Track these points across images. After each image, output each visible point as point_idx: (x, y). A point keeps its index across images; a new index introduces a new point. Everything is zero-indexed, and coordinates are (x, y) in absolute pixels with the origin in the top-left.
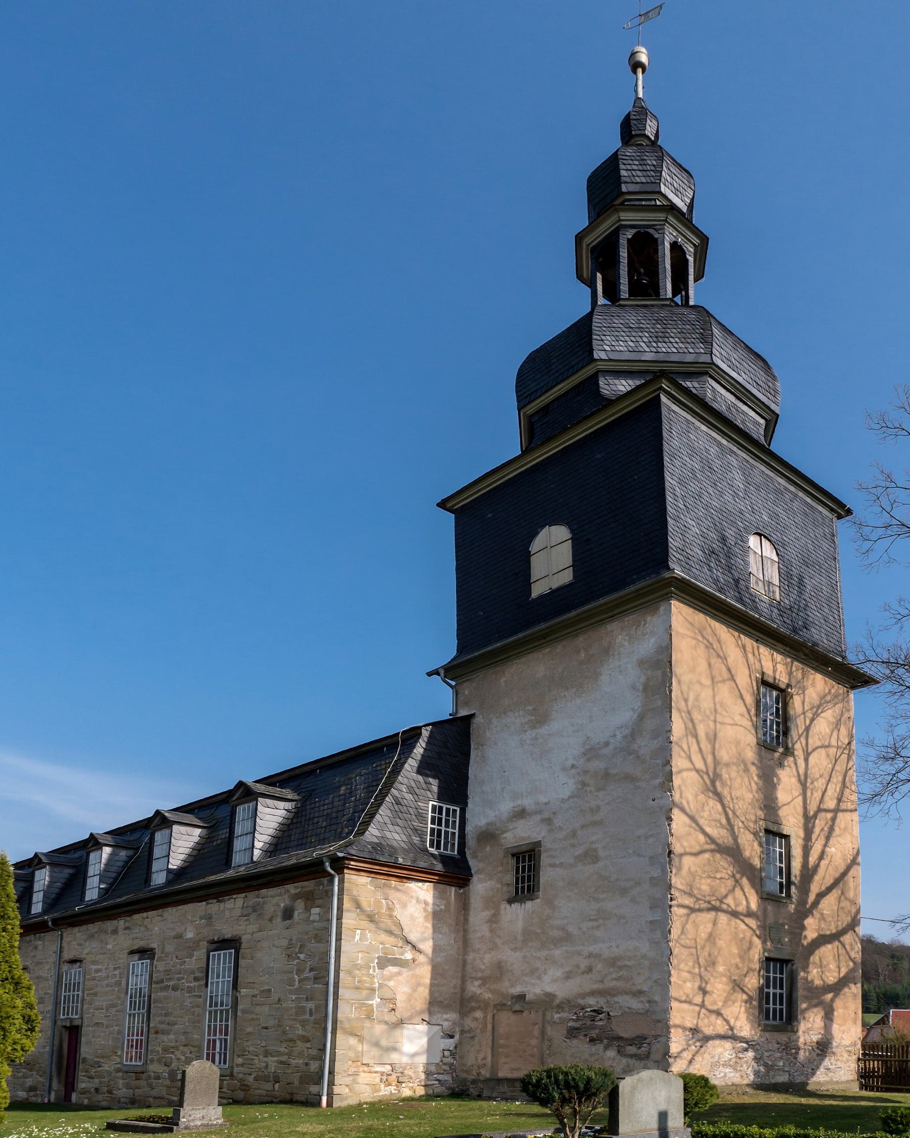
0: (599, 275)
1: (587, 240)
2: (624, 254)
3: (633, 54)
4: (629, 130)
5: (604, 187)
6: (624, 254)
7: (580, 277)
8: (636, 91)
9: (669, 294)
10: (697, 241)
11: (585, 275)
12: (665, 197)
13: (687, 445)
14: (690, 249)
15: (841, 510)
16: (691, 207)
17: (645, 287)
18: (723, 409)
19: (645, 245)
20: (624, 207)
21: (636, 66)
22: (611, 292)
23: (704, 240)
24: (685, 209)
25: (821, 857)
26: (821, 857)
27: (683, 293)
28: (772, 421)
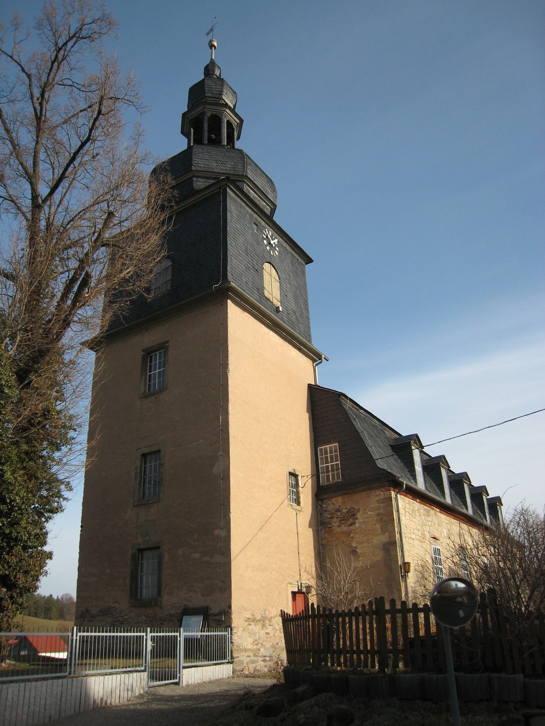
0: (192, 130)
1: (188, 116)
2: (206, 125)
3: (211, 41)
4: (209, 70)
5: (197, 93)
6: (206, 125)
7: (183, 132)
8: (212, 56)
9: (226, 144)
10: (238, 122)
11: (185, 132)
12: (224, 100)
13: (237, 213)
14: (235, 125)
15: (309, 260)
16: (235, 106)
17: (215, 142)
18: (252, 197)
19: (216, 121)
20: (206, 103)
21: (212, 46)
22: (198, 141)
23: (242, 121)
24: (232, 106)
25: (53, 219)
26: (53, 219)
27: (231, 144)
28: (273, 211)
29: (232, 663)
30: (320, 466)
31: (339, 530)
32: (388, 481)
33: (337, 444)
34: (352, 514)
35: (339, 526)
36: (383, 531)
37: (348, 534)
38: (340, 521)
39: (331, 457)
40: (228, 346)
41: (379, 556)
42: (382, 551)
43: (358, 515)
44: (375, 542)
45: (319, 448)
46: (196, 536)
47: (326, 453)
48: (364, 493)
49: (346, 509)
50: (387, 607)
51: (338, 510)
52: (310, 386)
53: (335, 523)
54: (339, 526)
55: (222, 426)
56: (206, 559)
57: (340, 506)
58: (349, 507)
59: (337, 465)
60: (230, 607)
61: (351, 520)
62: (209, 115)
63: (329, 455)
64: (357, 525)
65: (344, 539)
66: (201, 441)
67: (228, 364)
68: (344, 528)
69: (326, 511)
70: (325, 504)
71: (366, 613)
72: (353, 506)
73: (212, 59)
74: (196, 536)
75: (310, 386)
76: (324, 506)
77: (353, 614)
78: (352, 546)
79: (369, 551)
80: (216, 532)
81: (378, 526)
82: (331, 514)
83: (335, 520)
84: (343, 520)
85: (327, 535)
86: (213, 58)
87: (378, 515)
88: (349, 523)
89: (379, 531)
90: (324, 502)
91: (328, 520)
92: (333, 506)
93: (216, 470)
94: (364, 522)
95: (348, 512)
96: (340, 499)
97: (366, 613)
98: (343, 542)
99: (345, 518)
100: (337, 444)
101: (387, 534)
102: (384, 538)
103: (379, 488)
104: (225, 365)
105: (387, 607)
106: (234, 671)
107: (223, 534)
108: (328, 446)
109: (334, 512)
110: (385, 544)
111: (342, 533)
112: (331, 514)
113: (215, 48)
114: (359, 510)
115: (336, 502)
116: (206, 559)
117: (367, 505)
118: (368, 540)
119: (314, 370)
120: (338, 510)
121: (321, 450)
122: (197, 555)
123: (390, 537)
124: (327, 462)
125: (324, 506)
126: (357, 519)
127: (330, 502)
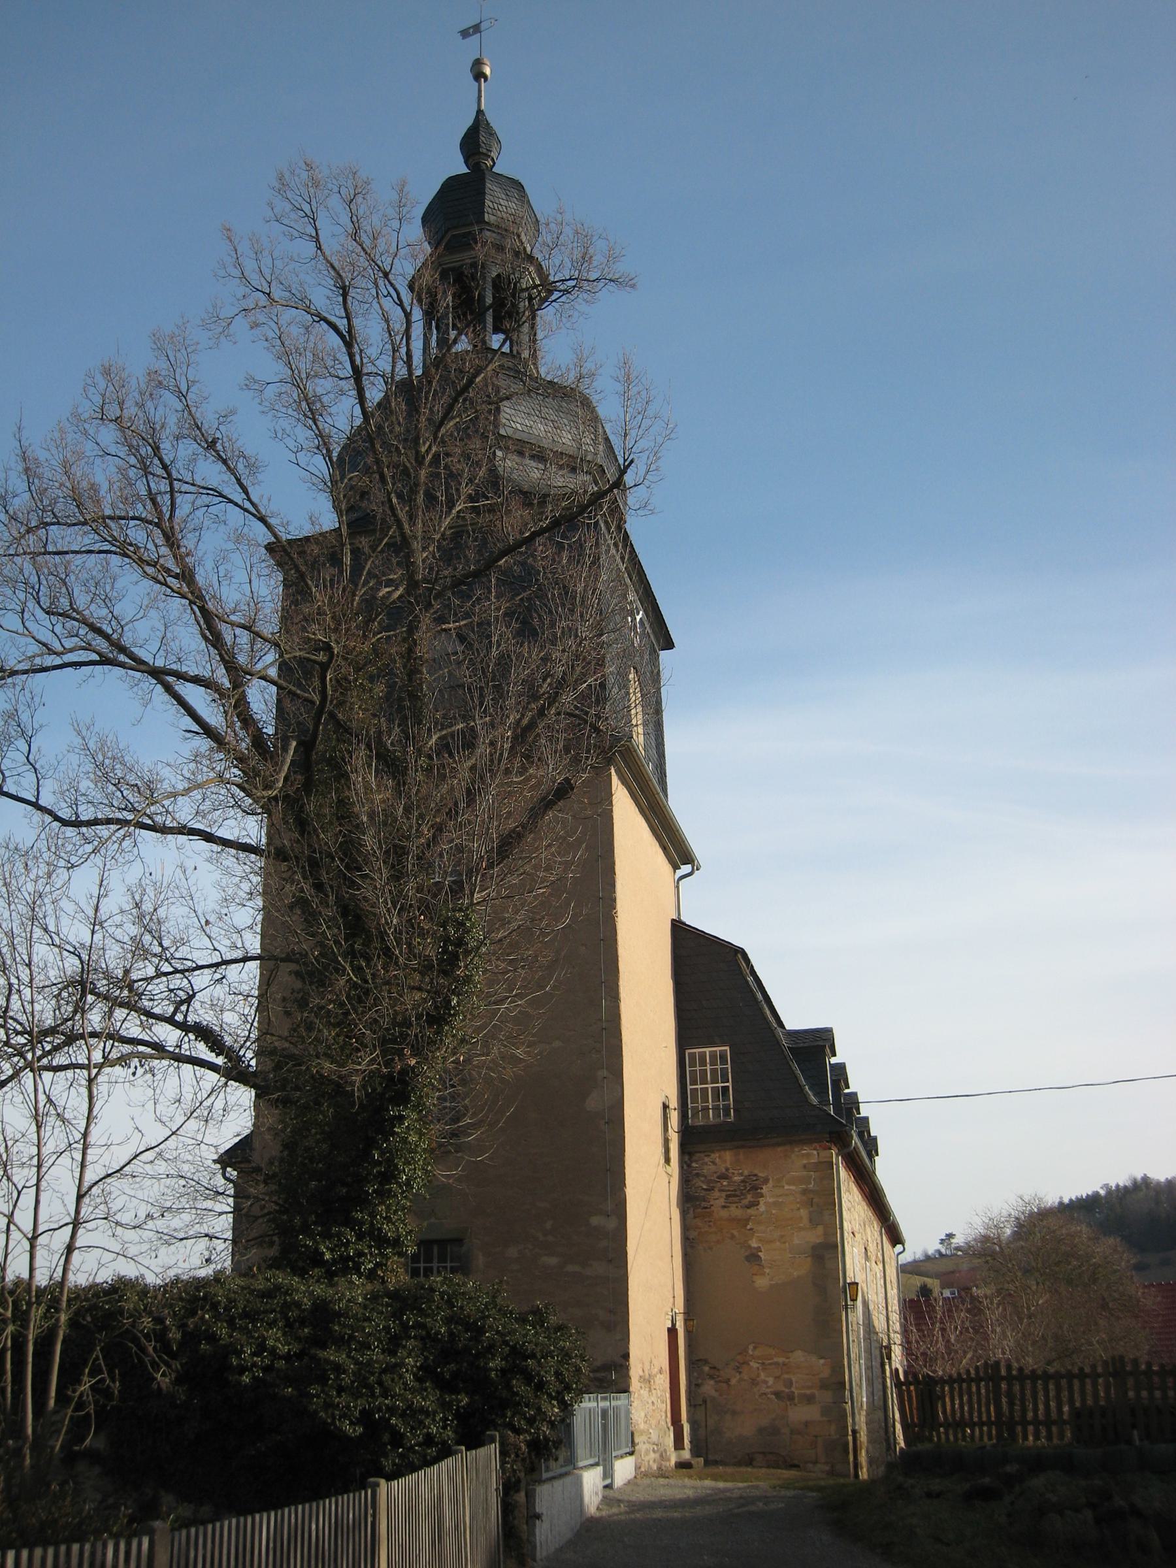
4: (476, 141)
15: (669, 644)
21: (479, 76)
29: (631, 1453)
30: (689, 1087)
31: (724, 1213)
32: (830, 1133)
33: (727, 1048)
34: (753, 1186)
35: (724, 1207)
36: (814, 1222)
37: (743, 1222)
38: (728, 1196)
39: (714, 1071)
40: (614, 863)
41: (802, 1268)
42: (809, 1259)
43: (765, 1190)
44: (796, 1241)
45: (687, 1052)
46: (549, 1225)
47: (703, 1063)
48: (780, 1149)
49: (741, 1174)
50: (1003, 1372)
51: (723, 1177)
52: (673, 920)
53: (717, 1200)
54: (724, 1207)
55: (607, 1021)
56: (570, 1268)
57: (727, 1169)
58: (746, 1173)
59: (725, 1089)
60: (626, 1356)
61: (749, 1198)
62: (494, 274)
63: (708, 1067)
64: (762, 1208)
65: (735, 1233)
66: (557, 1044)
67: (614, 900)
68: (735, 1211)
69: (698, 1175)
70: (696, 1161)
71: (972, 1380)
72: (756, 1172)
73: (480, 112)
74: (549, 1225)
75: (673, 920)
76: (694, 1165)
77: (955, 1381)
78: (750, 1247)
79: (782, 1258)
80: (595, 1221)
81: (804, 1213)
82: (709, 1182)
83: (716, 1194)
84: (733, 1196)
85: (698, 1222)
86: (483, 107)
87: (804, 1192)
88: (745, 1202)
89: (806, 1221)
90: (694, 1158)
91: (703, 1193)
92: (713, 1167)
93: (593, 1103)
94: (775, 1204)
95: (743, 1181)
96: (728, 1156)
97: (981, 1380)
98: (733, 1237)
99: (738, 1193)
100: (727, 1048)
101: (820, 1229)
102: (815, 1236)
103: (809, 1142)
104: (611, 902)
105: (1003, 1372)
106: (637, 1468)
107: (612, 1224)
108: (707, 1050)
109: (714, 1178)
110: (815, 1248)
111: (731, 1220)
112: (709, 1182)
113: (486, 80)
114: (766, 1181)
115: (722, 1160)
116: (570, 1268)
117: (785, 1173)
118: (782, 1236)
119: (678, 887)
120: (723, 1177)
121: (692, 1056)
122: (553, 1261)
123: (826, 1234)
124: (704, 1081)
125: (694, 1165)
126: (762, 1196)
127: (706, 1159)
